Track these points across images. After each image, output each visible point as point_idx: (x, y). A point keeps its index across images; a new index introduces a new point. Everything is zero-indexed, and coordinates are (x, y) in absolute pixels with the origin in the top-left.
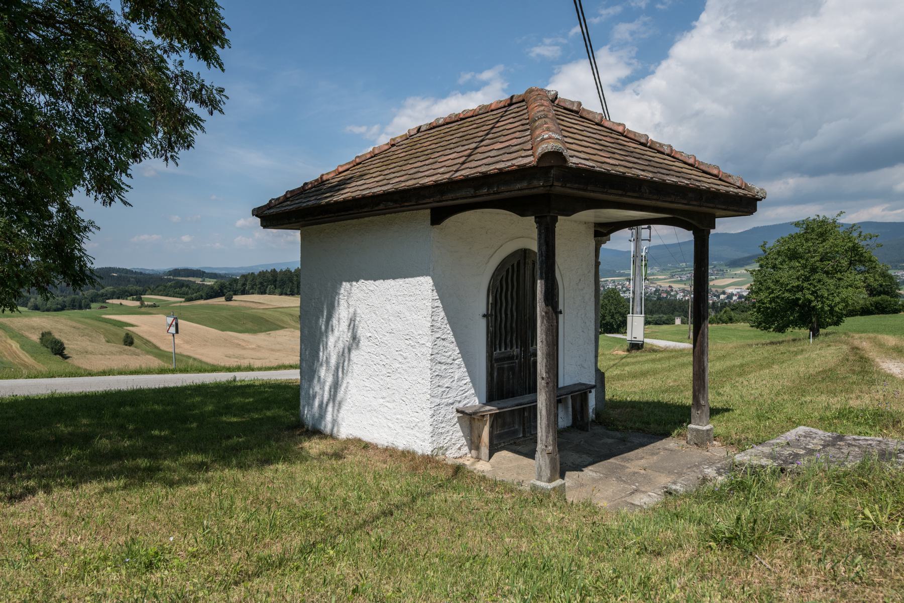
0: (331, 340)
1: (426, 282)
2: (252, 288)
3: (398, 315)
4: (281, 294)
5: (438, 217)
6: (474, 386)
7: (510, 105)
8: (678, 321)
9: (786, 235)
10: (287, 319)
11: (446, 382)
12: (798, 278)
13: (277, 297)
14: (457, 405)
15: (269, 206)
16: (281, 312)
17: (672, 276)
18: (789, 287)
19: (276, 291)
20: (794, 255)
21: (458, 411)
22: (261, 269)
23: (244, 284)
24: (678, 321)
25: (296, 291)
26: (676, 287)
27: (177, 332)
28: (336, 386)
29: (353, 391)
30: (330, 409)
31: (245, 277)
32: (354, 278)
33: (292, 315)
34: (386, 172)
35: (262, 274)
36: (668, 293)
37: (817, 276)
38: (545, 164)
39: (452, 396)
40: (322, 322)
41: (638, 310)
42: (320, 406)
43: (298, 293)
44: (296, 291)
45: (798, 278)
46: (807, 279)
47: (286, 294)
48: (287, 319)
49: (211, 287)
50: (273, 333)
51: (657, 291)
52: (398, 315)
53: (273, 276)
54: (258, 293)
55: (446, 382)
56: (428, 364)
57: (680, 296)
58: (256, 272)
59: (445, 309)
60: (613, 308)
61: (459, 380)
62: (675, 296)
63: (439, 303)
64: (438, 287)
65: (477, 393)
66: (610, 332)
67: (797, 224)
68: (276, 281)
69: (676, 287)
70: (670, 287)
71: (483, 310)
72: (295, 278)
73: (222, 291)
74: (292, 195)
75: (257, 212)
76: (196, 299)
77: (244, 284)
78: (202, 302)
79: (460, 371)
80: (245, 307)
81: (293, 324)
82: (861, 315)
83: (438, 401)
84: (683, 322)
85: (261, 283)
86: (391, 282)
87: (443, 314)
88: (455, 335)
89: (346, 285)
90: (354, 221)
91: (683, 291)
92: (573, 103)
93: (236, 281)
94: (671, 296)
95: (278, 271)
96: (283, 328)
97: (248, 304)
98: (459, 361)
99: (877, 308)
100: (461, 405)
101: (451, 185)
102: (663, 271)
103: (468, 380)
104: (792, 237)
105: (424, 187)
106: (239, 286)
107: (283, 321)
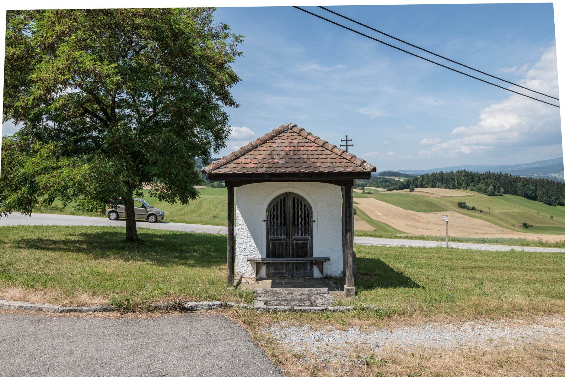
2: (427, 184)
4: (446, 188)
6: (259, 249)
10: (449, 204)
13: (443, 190)
14: (249, 256)
16: (445, 200)
19: (443, 186)
23: (422, 181)
33: (452, 202)
35: (434, 175)
47: (450, 188)
49: (402, 183)
50: (439, 213)
53: (441, 176)
54: (431, 187)
58: (430, 174)
61: (250, 246)
65: (261, 253)
68: (443, 179)
72: (456, 177)
77: (422, 181)
78: (396, 191)
81: (453, 208)
85: (433, 181)
87: (242, 219)
88: (248, 227)
93: (417, 179)
95: (444, 172)
96: (446, 210)
97: (421, 194)
103: (256, 247)
106: (419, 182)
107: (446, 206)
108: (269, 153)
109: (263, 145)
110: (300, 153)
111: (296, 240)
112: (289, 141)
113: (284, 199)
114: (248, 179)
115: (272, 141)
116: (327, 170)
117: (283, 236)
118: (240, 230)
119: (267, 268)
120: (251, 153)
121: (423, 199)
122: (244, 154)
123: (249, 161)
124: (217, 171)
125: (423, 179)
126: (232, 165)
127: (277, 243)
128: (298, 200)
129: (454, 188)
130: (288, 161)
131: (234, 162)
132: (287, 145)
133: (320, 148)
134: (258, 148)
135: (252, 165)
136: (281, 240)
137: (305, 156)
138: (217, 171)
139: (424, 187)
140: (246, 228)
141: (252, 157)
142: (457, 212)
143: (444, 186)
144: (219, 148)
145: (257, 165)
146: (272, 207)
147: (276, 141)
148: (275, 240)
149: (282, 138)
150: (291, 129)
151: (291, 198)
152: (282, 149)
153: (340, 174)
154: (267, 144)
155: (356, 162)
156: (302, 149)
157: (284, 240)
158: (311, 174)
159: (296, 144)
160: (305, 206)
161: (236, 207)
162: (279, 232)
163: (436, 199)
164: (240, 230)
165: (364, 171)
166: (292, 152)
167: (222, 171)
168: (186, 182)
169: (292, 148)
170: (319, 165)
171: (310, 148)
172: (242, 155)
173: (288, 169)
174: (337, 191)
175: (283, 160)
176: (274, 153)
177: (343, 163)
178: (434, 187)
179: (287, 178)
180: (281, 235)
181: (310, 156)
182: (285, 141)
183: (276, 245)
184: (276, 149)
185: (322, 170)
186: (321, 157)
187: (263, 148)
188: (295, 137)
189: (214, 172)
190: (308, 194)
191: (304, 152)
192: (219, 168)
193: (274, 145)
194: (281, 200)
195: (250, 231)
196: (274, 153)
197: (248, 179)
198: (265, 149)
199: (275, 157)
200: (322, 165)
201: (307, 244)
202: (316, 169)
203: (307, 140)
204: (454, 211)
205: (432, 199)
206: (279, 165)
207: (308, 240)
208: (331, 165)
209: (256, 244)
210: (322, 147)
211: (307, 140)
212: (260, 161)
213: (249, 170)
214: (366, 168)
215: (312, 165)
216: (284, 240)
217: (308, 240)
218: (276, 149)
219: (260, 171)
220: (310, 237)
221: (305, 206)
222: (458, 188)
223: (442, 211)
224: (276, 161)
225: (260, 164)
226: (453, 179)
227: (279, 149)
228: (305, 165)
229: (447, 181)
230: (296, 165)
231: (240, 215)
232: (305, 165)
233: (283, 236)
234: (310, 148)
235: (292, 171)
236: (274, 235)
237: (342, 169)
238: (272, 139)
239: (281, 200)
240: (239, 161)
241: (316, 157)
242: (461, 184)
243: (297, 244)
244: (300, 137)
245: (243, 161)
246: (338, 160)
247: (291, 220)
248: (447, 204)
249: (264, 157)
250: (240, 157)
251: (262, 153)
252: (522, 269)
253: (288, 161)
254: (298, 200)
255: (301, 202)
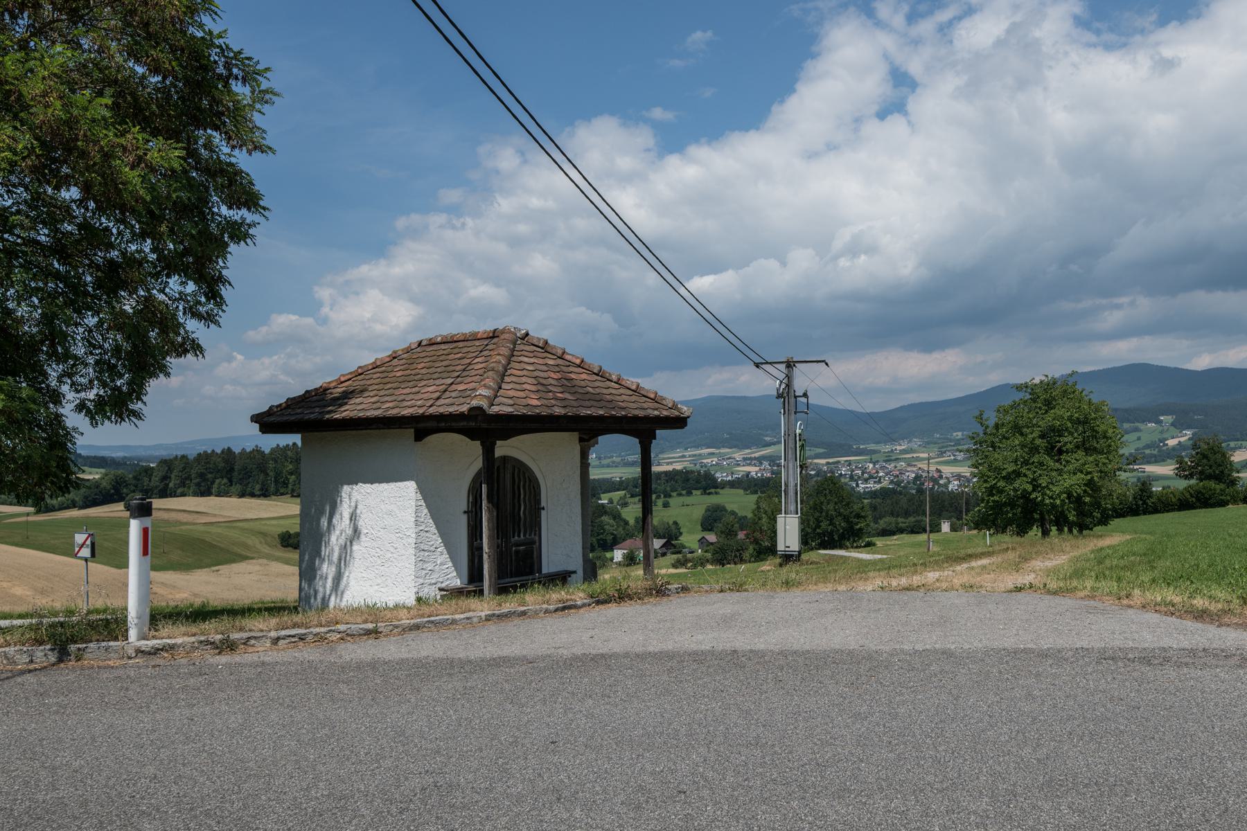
0: (333, 538)
1: (410, 487)
2: (183, 484)
3: (390, 513)
4: (242, 495)
5: (420, 436)
6: (456, 569)
7: (493, 337)
8: (946, 527)
9: (1007, 402)
10: (253, 541)
11: (430, 566)
12: (1015, 461)
13: (234, 501)
14: (439, 585)
15: (270, 412)
16: (243, 529)
17: (941, 454)
18: (1004, 473)
19: (233, 489)
20: (1017, 429)
21: (441, 590)
22: (201, 449)
23: (165, 478)
24: (946, 527)
25: (272, 488)
26: (947, 470)
27: (93, 554)
28: (338, 577)
29: (352, 583)
30: (333, 598)
31: (167, 464)
32: (353, 481)
33: (264, 534)
34: (382, 393)
35: (204, 458)
36: (935, 481)
37: (1036, 459)
38: (472, 413)
39: (434, 578)
40: (324, 522)
41: (792, 508)
42: (323, 599)
43: (298, 496)
44: (272, 488)
45: (1015, 461)
46: (1026, 463)
47: (253, 495)
48: (253, 541)
49: (96, 484)
50: (224, 569)
51: (917, 477)
52: (390, 513)
53: (226, 461)
54: (195, 494)
55: (430, 566)
56: (412, 551)
57: (953, 486)
58: (192, 454)
59: (428, 507)
60: (831, 507)
61: (441, 564)
62: (946, 485)
63: (422, 503)
64: (422, 489)
65: (459, 575)
66: (825, 548)
67: (1019, 388)
68: (232, 469)
69: (947, 470)
70: (938, 471)
71: (464, 507)
72: (271, 465)
73: (118, 492)
74: (292, 403)
75: (256, 418)
76: (63, 507)
77: (165, 478)
78: (75, 513)
79: (443, 557)
80: (167, 521)
81: (267, 550)
82: (1180, 509)
83: (421, 581)
84: (954, 529)
85: (202, 475)
86: (384, 485)
87: (426, 511)
88: (437, 528)
89: (346, 488)
90: (354, 432)
91: (959, 477)
92: (539, 339)
93: (148, 471)
94: (940, 485)
95: (237, 450)
96: (244, 558)
97: (173, 516)
98: (442, 549)
99: (1198, 499)
100: (443, 585)
101: (423, 418)
102: (926, 445)
103: (450, 564)
104: (1014, 406)
105: (403, 417)
106: (155, 481)
107: (246, 547)
119: (774, 545)
121: (172, 529)
125: (170, 470)
129: (265, 494)
139: (173, 495)
140: (433, 529)
142: (278, 559)
143: (236, 488)
163: (214, 530)
174: (632, 443)
178: (205, 492)
204: (269, 557)
205: (202, 528)
209: (451, 558)
222: (278, 493)
223: (234, 561)
226: (263, 469)
229: (246, 475)
242: (285, 484)
248: (250, 542)
252: (1000, 552)
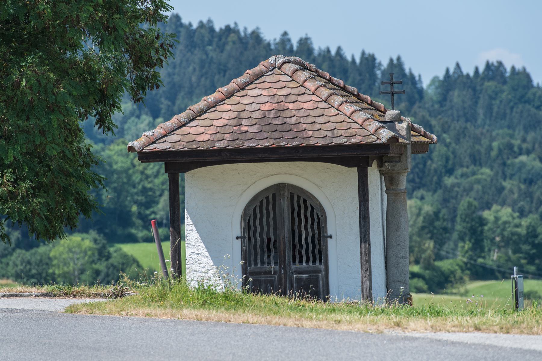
87: (197, 235)
88: (209, 250)
108: (234, 115)
109: (227, 101)
110: (287, 113)
111: (298, 272)
112: (273, 91)
113: (274, 196)
114: (200, 159)
115: (242, 93)
116: (321, 142)
117: (273, 265)
118: (194, 256)
120: (204, 116)
122: (194, 119)
123: (202, 130)
124: (151, 147)
126: (174, 137)
127: (263, 278)
128: (299, 197)
130: (264, 128)
131: (177, 132)
132: (267, 99)
133: (323, 105)
134: (218, 108)
135: (205, 137)
136: (269, 272)
137: (293, 120)
138: (151, 147)
140: (205, 252)
141: (266, 85)
144: (144, 89)
145: (213, 136)
146: (251, 212)
147: (250, 93)
148: (259, 273)
149: (260, 86)
150: (280, 68)
151: (287, 193)
152: (258, 106)
153: (341, 147)
154: (235, 99)
155: (369, 128)
156: (291, 106)
157: (275, 273)
158: (296, 148)
159: (283, 98)
160: (313, 209)
161: (188, 221)
162: (266, 256)
164: (193, 255)
165: (378, 142)
166: (273, 112)
167: (159, 147)
168: (68, 175)
169: (274, 106)
170: (310, 133)
171: (305, 106)
172: (191, 121)
173: (261, 142)
175: (257, 126)
176: (244, 115)
177: (350, 131)
179: (260, 155)
180: (269, 264)
181: (302, 120)
182: (265, 93)
183: (260, 281)
184: (248, 108)
185: (312, 142)
186: (319, 120)
187: (226, 107)
188: (284, 84)
189: (146, 149)
190: (318, 186)
191: (294, 112)
192: (154, 143)
193: (245, 100)
194: (267, 198)
195: (213, 258)
196: (244, 115)
197: (200, 159)
198: (229, 107)
199: (244, 122)
200: (317, 134)
201: (317, 280)
202: (304, 141)
203: (303, 90)
206: (249, 136)
207: (320, 271)
208: (329, 134)
210: (325, 102)
211: (303, 90)
212: (219, 129)
213: (201, 144)
214: (381, 137)
215: (300, 135)
216: (275, 273)
217: (320, 271)
218: (248, 108)
219: (218, 145)
220: (322, 267)
221: (313, 209)
224: (244, 128)
225: (218, 135)
227: (254, 107)
228: (290, 135)
230: (276, 135)
231: (193, 227)
232: (290, 135)
233: (273, 265)
234: (305, 106)
235: (253, 145)
236: (256, 264)
237: (345, 140)
238: (243, 89)
239: (267, 198)
240: (185, 130)
241: (310, 120)
243: (298, 280)
244: (292, 85)
245: (192, 130)
246: (344, 126)
247: (287, 236)
249: (226, 122)
250: (187, 123)
251: (224, 115)
253: (264, 128)
254: (299, 197)
255: (305, 201)
